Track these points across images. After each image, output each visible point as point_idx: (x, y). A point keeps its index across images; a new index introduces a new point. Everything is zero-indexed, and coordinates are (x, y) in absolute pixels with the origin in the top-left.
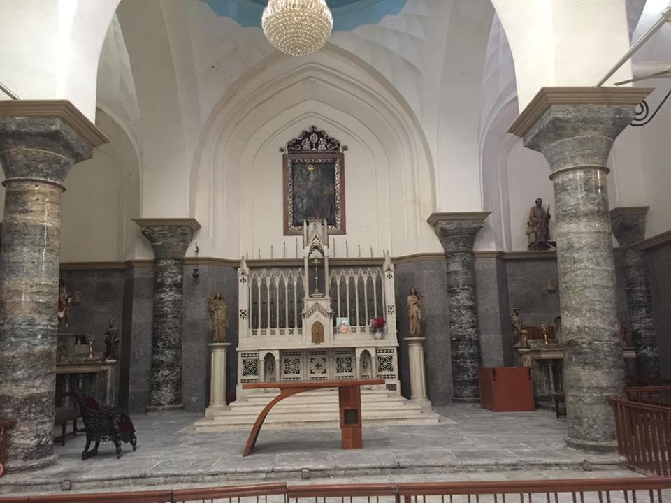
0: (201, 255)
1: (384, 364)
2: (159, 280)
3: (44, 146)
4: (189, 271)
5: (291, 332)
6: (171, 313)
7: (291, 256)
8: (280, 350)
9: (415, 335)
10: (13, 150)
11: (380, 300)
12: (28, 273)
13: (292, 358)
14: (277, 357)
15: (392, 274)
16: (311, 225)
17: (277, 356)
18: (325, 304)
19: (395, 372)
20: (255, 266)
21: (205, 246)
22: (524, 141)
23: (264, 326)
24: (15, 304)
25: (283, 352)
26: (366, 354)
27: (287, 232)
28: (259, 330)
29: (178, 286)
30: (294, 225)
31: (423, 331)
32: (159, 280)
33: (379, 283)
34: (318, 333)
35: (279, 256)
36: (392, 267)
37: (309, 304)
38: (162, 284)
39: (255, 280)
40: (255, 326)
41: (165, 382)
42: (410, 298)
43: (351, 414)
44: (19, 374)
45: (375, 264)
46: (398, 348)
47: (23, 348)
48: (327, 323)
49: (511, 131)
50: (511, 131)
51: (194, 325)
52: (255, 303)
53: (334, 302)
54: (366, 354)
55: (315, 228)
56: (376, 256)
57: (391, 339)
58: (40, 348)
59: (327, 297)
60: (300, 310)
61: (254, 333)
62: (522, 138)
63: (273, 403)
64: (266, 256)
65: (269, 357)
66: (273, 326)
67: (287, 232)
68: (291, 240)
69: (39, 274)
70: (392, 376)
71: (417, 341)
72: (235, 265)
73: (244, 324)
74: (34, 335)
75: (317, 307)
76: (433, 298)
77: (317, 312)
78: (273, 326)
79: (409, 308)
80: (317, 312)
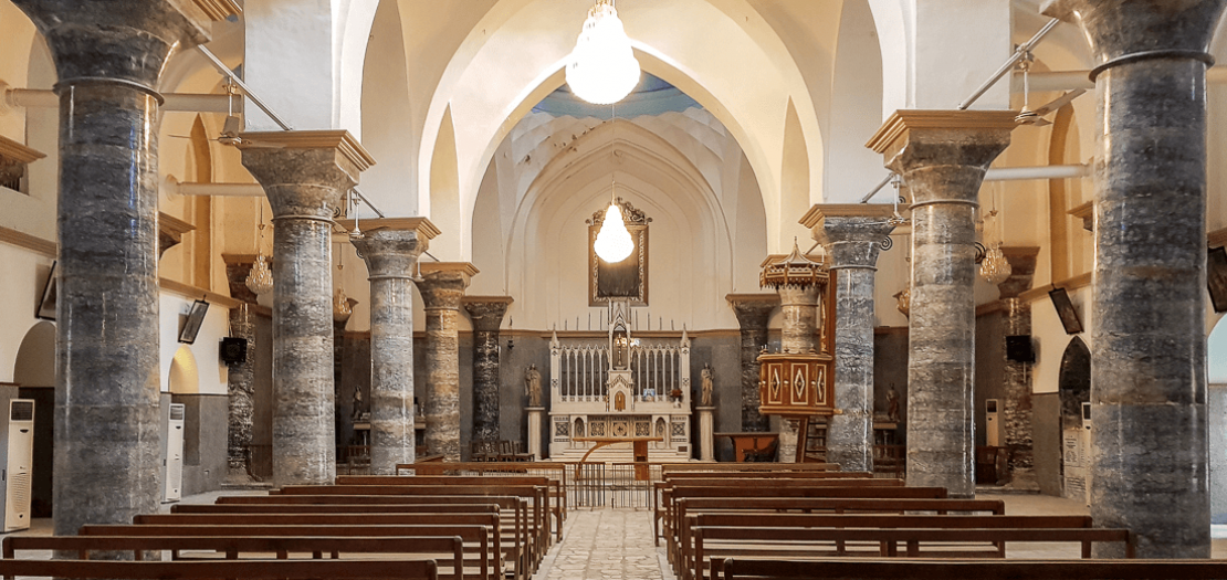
0: (513, 328)
1: (677, 429)
2: (479, 350)
3: (452, 287)
4: (504, 341)
5: (597, 399)
6: (491, 379)
7: (595, 328)
8: (589, 416)
9: (706, 405)
10: (434, 290)
11: (676, 372)
12: (445, 367)
13: (598, 422)
14: (585, 421)
15: (688, 350)
16: (616, 305)
17: (585, 419)
18: (627, 376)
19: (687, 436)
20: (565, 337)
21: (513, 321)
22: (886, 159)
23: (572, 394)
24: (440, 386)
25: (590, 417)
26: (661, 420)
27: (592, 303)
28: (568, 397)
29: (494, 355)
30: (598, 296)
31: (715, 400)
32: (479, 350)
33: (677, 356)
34: (620, 403)
35: (583, 327)
36: (688, 344)
37: (612, 376)
38: (483, 354)
39: (564, 353)
40: (564, 393)
41: (487, 440)
42: (703, 372)
43: (640, 449)
44: (444, 427)
45: (674, 337)
46: (690, 416)
47: (445, 412)
48: (628, 392)
49: (802, 222)
50: (802, 222)
51: (508, 389)
52: (564, 373)
53: (635, 375)
54: (661, 420)
55: (619, 305)
56: (676, 329)
57: (686, 409)
58: (454, 412)
59: (629, 369)
60: (604, 381)
61: (564, 400)
62: (882, 155)
63: (591, 451)
64: (572, 328)
65: (579, 421)
66: (581, 393)
67: (592, 303)
68: (596, 310)
69: (451, 368)
70: (684, 440)
71: (707, 410)
72: (547, 336)
73: (555, 392)
74: (450, 405)
75: (620, 379)
76: (727, 366)
77: (620, 383)
78: (589, 393)
79: (701, 381)
80: (620, 383)
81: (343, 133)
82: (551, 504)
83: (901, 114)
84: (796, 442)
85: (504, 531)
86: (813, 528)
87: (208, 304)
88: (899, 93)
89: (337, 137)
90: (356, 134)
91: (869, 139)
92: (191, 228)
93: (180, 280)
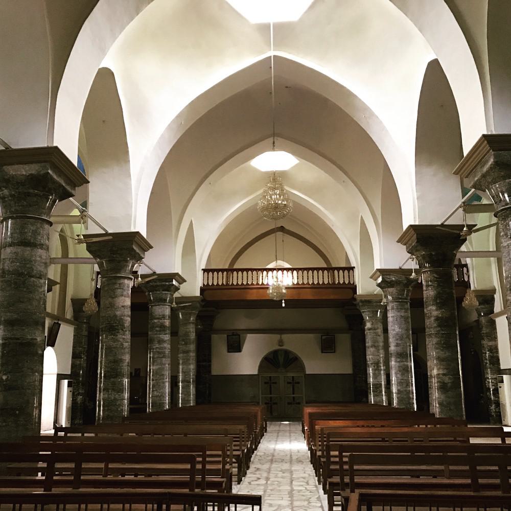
81: (138, 233)
82: (60, 507)
83: (411, 226)
84: (56, 508)
85: (218, 462)
86: (437, 454)
87: (60, 324)
88: (410, 218)
89: (133, 237)
90: (144, 234)
91: (397, 239)
92: (57, 283)
93: (251, 508)
